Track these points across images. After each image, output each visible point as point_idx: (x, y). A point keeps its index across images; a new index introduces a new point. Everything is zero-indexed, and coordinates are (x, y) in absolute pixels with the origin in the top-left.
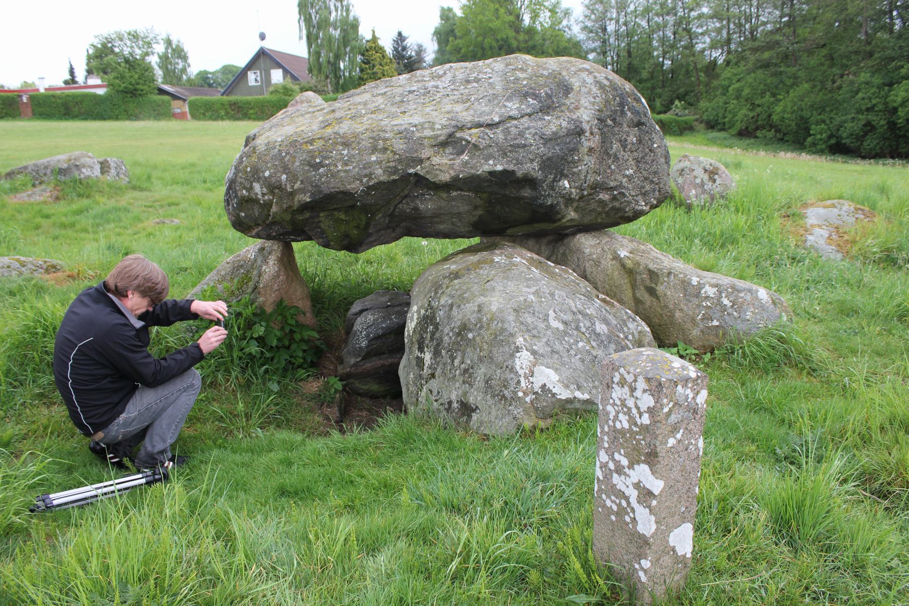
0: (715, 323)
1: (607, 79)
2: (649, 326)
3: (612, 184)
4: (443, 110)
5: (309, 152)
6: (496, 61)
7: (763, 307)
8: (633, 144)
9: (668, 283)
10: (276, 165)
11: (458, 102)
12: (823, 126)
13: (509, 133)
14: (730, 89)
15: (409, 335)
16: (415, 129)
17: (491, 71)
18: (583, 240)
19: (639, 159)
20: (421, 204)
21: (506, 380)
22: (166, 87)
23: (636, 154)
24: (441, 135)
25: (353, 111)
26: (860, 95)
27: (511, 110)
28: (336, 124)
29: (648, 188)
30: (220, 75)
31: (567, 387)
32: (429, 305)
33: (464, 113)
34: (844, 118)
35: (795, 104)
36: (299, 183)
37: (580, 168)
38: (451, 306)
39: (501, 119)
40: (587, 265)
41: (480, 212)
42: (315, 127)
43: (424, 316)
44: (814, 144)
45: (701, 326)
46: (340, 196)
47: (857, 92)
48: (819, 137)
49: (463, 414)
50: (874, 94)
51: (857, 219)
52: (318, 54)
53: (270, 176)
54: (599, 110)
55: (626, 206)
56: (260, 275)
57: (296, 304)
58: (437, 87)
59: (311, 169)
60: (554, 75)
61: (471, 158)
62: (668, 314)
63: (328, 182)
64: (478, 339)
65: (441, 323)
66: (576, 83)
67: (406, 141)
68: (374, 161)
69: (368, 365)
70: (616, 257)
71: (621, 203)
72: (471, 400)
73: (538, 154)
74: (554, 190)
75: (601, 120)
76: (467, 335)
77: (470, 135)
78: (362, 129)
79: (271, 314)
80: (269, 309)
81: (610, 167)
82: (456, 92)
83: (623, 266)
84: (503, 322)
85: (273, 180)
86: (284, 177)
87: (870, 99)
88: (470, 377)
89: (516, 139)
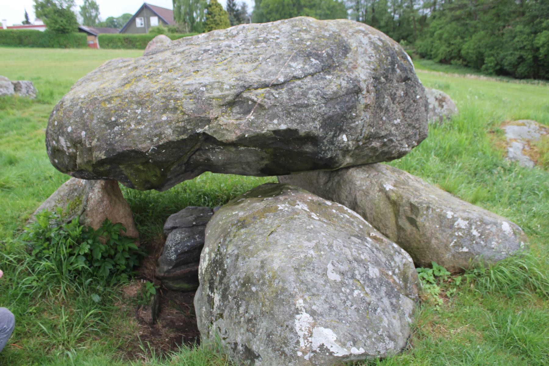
0: (465, 250)
1: (380, 40)
2: (410, 253)
3: (383, 133)
4: (233, 69)
5: (107, 110)
6: (283, 23)
7: (505, 238)
8: (401, 97)
9: (427, 216)
10: (77, 122)
11: (247, 61)
12: (492, 58)
13: (293, 93)
14: (436, 34)
15: (202, 273)
16: (204, 89)
17: (278, 32)
18: (355, 173)
19: (405, 110)
20: (213, 156)
21: (286, 338)
22: (85, 28)
23: (402, 105)
24: (228, 96)
25: (152, 69)
26: (516, 39)
27: (296, 70)
28: (135, 81)
29: (411, 132)
30: (122, 20)
31: (343, 345)
32: (218, 250)
33: (252, 73)
34: (506, 53)
35: (476, 44)
36: (96, 140)
37: (357, 123)
38: (237, 256)
39: (286, 79)
40: (358, 194)
41: (266, 162)
42: (116, 85)
43: (214, 260)
44: (487, 69)
45: (453, 251)
46: (133, 154)
47: (514, 37)
48: (489, 65)
49: (247, 358)
50: (525, 38)
51: (542, 134)
52: (179, 7)
53: (72, 132)
54: (374, 69)
55: (393, 150)
56: (87, 201)
57: (120, 221)
58: (229, 46)
59: (107, 128)
60: (334, 36)
61: (257, 117)
62: (425, 240)
63: (121, 141)
64: (260, 293)
65: (228, 270)
66: (353, 43)
67: (196, 101)
68: (165, 121)
69: (178, 272)
70: (382, 190)
71: (389, 148)
72: (254, 348)
73: (320, 113)
74: (334, 144)
75: (376, 79)
76: (250, 288)
77: (257, 95)
78: (156, 88)
79: (98, 231)
80: (96, 227)
81: (382, 119)
82: (246, 52)
83: (388, 198)
84: (284, 282)
85: (74, 136)
86: (83, 133)
87: (522, 42)
88: (253, 326)
89: (299, 99)
